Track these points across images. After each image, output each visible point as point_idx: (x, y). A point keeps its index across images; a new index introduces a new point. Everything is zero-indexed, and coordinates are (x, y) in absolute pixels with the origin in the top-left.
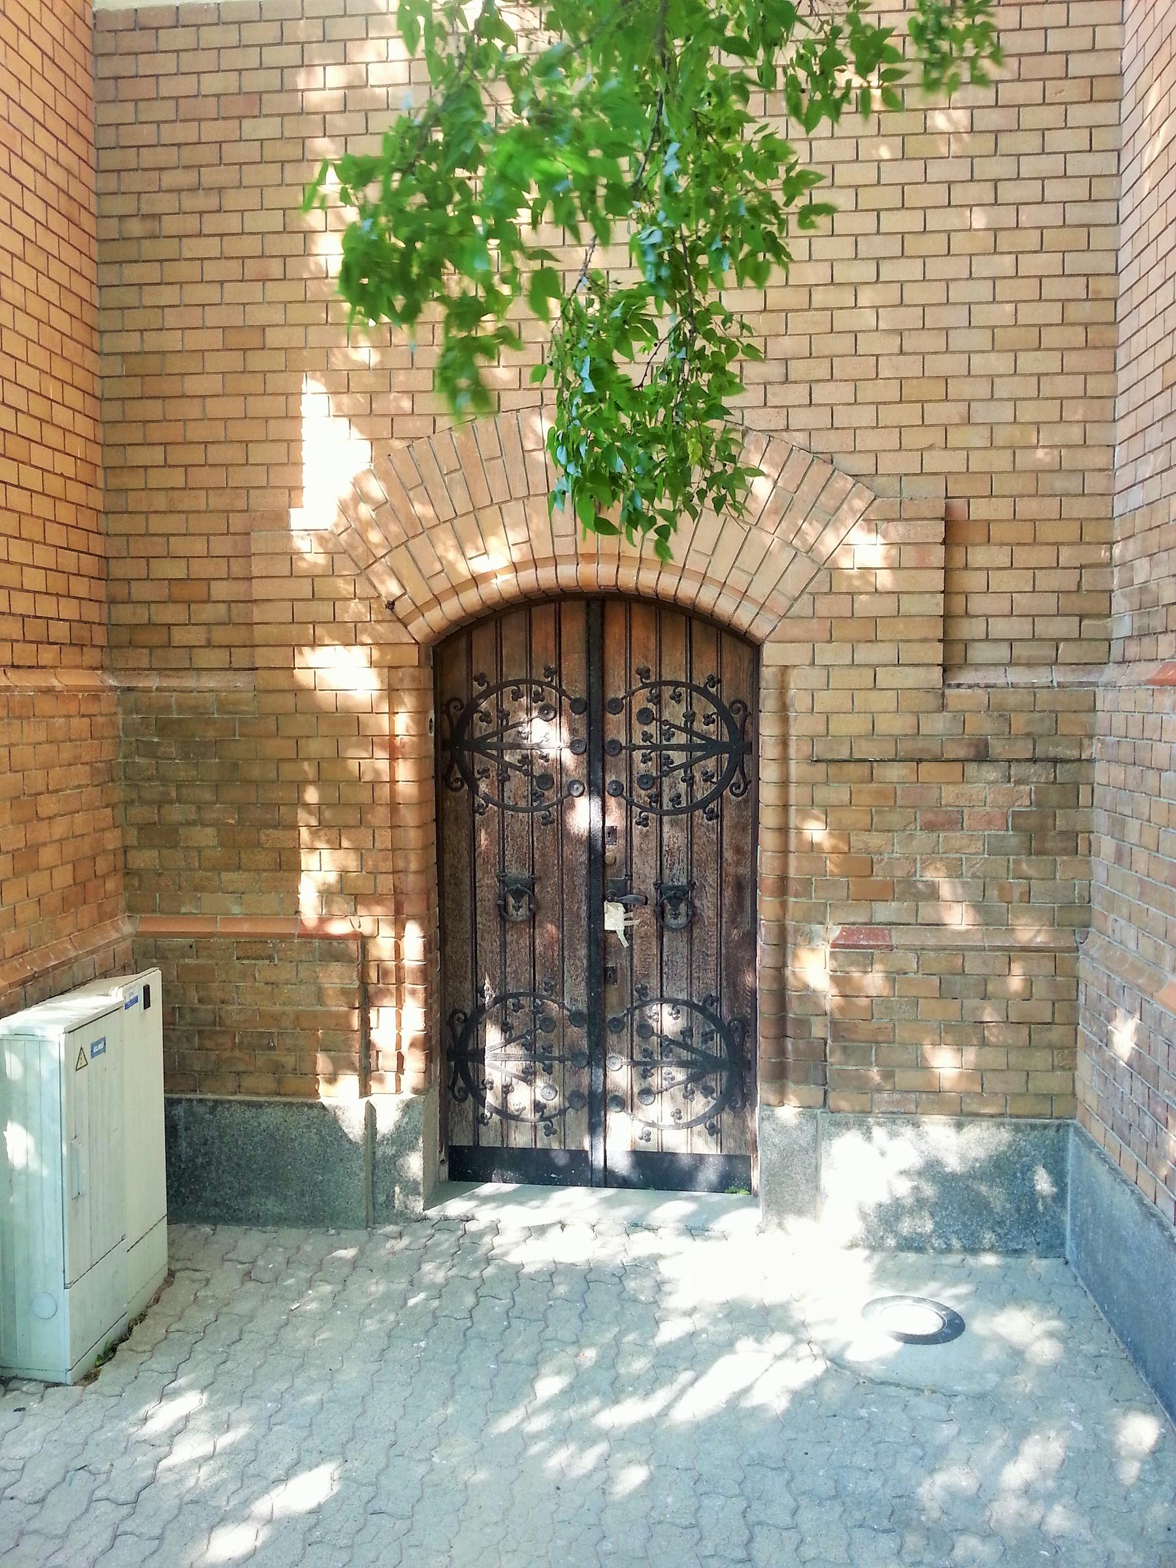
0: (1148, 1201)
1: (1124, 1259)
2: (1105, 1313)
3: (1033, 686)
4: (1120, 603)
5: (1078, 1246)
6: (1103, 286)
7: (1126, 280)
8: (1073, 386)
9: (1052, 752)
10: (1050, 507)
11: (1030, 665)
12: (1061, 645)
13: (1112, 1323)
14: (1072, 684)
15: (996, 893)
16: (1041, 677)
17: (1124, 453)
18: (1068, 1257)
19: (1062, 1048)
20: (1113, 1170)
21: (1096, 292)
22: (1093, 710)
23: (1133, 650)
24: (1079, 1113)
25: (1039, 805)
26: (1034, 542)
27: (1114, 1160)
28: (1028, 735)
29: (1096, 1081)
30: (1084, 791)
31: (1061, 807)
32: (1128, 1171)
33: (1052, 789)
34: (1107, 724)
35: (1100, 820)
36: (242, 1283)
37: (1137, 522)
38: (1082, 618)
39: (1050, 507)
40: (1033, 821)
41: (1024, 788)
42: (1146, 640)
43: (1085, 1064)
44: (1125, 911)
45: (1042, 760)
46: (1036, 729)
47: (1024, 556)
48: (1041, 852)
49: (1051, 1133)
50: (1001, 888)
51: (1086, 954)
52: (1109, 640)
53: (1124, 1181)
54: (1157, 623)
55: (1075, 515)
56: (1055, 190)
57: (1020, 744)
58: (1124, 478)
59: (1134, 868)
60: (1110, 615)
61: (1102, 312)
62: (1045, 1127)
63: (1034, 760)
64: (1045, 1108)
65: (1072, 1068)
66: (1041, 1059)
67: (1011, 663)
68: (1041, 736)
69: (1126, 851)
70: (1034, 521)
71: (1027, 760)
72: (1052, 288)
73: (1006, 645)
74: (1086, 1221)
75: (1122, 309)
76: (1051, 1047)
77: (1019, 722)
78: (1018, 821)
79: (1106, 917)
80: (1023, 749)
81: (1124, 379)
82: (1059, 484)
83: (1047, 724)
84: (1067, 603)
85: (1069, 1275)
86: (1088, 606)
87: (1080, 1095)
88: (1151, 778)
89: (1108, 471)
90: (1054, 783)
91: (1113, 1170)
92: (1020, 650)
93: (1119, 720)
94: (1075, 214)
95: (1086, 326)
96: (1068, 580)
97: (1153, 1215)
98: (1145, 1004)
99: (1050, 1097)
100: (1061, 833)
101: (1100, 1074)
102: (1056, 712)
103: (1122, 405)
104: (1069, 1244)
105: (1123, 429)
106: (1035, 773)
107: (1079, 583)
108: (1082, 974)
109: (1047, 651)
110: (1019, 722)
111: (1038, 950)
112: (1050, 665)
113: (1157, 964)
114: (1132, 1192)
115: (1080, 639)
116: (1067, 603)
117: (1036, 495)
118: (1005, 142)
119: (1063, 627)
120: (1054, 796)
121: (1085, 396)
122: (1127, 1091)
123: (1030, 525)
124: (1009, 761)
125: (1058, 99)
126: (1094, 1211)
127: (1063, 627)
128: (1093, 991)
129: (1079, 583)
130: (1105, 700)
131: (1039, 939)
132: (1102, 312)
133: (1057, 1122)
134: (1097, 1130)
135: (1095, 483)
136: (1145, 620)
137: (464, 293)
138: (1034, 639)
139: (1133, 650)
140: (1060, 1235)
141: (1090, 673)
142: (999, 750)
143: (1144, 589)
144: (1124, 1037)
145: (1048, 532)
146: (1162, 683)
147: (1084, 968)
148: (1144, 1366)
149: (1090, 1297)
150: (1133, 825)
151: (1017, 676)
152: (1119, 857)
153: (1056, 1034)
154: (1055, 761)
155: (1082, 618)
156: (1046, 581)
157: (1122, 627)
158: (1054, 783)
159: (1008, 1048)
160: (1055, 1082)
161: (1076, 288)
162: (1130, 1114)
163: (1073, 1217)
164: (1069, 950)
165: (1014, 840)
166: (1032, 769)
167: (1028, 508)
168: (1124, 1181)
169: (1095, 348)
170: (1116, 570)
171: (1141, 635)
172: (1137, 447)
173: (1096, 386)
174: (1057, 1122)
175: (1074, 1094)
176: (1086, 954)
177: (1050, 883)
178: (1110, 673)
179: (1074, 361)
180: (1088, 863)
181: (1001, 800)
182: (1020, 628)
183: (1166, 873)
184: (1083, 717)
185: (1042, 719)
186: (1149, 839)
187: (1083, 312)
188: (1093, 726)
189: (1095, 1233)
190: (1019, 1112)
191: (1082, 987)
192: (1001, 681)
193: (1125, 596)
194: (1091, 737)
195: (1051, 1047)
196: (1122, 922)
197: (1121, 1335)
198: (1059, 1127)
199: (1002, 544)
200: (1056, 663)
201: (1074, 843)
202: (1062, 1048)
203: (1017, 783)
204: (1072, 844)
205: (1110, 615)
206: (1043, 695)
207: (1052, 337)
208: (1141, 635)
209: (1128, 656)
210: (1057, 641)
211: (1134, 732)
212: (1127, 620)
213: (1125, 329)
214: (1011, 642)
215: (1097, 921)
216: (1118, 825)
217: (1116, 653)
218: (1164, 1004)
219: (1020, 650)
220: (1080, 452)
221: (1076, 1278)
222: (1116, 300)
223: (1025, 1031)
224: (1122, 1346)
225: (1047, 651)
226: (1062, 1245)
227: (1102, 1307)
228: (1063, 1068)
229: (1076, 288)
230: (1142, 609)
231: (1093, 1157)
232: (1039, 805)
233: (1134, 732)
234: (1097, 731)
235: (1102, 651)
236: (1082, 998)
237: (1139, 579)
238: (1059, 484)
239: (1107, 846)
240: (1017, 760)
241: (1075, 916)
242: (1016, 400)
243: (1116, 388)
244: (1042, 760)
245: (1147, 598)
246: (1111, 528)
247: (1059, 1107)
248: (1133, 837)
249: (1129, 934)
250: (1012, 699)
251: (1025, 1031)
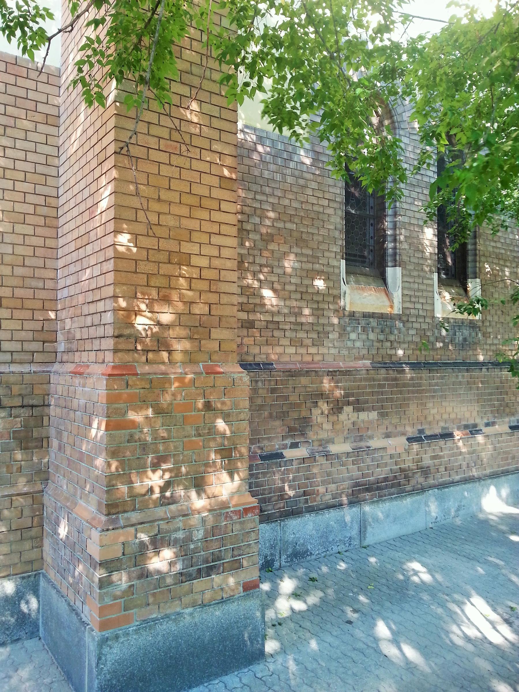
0: (72, 603)
1: (63, 632)
2: (56, 659)
3: (22, 373)
4: (60, 337)
5: (44, 629)
6: (52, 202)
7: (62, 201)
8: (40, 242)
9: (31, 402)
10: (29, 293)
11: (21, 363)
12: (35, 354)
13: (58, 663)
14: (40, 372)
15: (5, 469)
16: (26, 368)
17: (61, 273)
18: (41, 636)
19: (36, 538)
20: (58, 591)
21: (49, 203)
22: (49, 383)
23: (65, 358)
24: (45, 567)
25: (25, 427)
26: (22, 308)
27: (59, 587)
28: (20, 395)
29: (51, 552)
30: (46, 419)
31: (35, 427)
32: (64, 591)
33: (31, 419)
34: (54, 389)
35: (52, 432)
36: (103, 374)
37: (67, 303)
38: (44, 342)
39: (29, 293)
40: (22, 434)
41: (18, 419)
42: (70, 353)
43: (47, 543)
44: (62, 472)
45: (26, 406)
46: (23, 392)
47: (17, 314)
48: (26, 449)
49: (32, 579)
50: (8, 467)
51: (46, 493)
52: (56, 352)
53: (62, 596)
54: (74, 347)
55: (41, 297)
56: (31, 157)
57: (16, 399)
58: (61, 283)
59: (66, 453)
60: (56, 342)
61: (52, 212)
62: (29, 576)
63: (23, 407)
64: (29, 568)
65: (41, 546)
66: (27, 545)
67: (12, 362)
68: (26, 395)
69: (63, 446)
70: (22, 298)
71: (20, 406)
72: (30, 198)
73: (9, 354)
74: (47, 618)
75: (60, 213)
76: (32, 538)
77: (16, 389)
78: (16, 435)
79: (55, 475)
80: (18, 402)
81: (61, 242)
82: (34, 283)
83: (29, 390)
84: (37, 335)
85: (41, 645)
86: (47, 336)
87: (45, 559)
88: (72, 413)
89: (55, 279)
90: (32, 416)
91: (58, 591)
92: (16, 356)
93: (60, 388)
94: (40, 169)
95: (45, 217)
96: (38, 326)
97: (74, 610)
98: (70, 515)
99: (31, 562)
100: (36, 439)
101: (52, 548)
102: (33, 384)
103: (60, 253)
104: (41, 629)
105: (61, 263)
106: (23, 412)
107: (43, 327)
108: (45, 503)
109: (29, 357)
110: (16, 389)
111: (26, 494)
112: (30, 363)
113: (75, 495)
114: (66, 600)
115: (43, 352)
116: (37, 335)
117: (23, 287)
118: (9, 131)
119: (36, 346)
120: (32, 422)
121: (44, 247)
122: (63, 554)
123: (20, 300)
124: (11, 407)
125: (32, 119)
126: (51, 612)
127: (36, 346)
128: (50, 510)
129: (43, 327)
130: (53, 379)
131: (25, 489)
132: (52, 212)
133: (34, 573)
134: (52, 574)
135: (49, 284)
136: (70, 345)
137: (448, 215)
138: (22, 351)
139: (65, 358)
140: (37, 626)
141: (48, 367)
142: (5, 403)
143: (69, 332)
144: (63, 531)
145: (28, 304)
146: (75, 373)
147: (46, 499)
148: (71, 681)
149: (50, 653)
150: (65, 434)
151: (15, 368)
152: (60, 449)
153: (34, 532)
154: (32, 406)
155: (44, 342)
156: (28, 325)
157: (61, 347)
158: (32, 416)
159: (11, 543)
160: (33, 555)
161: (40, 200)
162: (64, 565)
163: (43, 616)
164: (39, 492)
165: (13, 443)
166: (22, 410)
167: (19, 293)
168: (62, 596)
169: (49, 227)
170: (59, 322)
171: (68, 351)
172: (66, 271)
173: (50, 243)
174: (34, 573)
175: (42, 558)
176: (46, 493)
177: (30, 462)
178: (56, 367)
179: (39, 231)
180: (48, 451)
181: (7, 426)
182: (17, 346)
183: (77, 456)
184: (45, 386)
185: (26, 388)
186: (71, 441)
187: (44, 211)
188: (49, 390)
189: (51, 622)
190: (17, 572)
191: (45, 508)
192: (7, 370)
193: (62, 334)
194: (48, 395)
195: (32, 538)
196: (61, 477)
197: (62, 668)
198: (35, 575)
199: (7, 308)
200: (32, 362)
201: (42, 443)
202: (36, 538)
203: (15, 417)
204: (39, 444)
205: (56, 342)
206: (26, 377)
207: (29, 219)
208: (68, 351)
209: (64, 360)
210: (33, 352)
211: (65, 394)
212: (63, 344)
213: (62, 221)
214: (12, 352)
215: (52, 477)
216: (59, 433)
217: (59, 358)
218: (77, 514)
219: (16, 356)
220: (42, 271)
221: (44, 645)
222: (57, 208)
223: (19, 533)
224: (62, 674)
225: (29, 357)
226: (38, 630)
227: (55, 657)
228: (37, 547)
229: (40, 200)
230: (69, 340)
231: (50, 587)
232: (25, 427)
233: (65, 394)
234: (51, 392)
235: (53, 357)
236: (45, 513)
237: (67, 327)
238: (34, 283)
239: (55, 443)
240: (15, 407)
241: (43, 475)
242: (13, 244)
243: (58, 245)
244: (26, 406)
245: (71, 336)
246: (57, 304)
247: (35, 566)
248: (65, 440)
249: (64, 482)
250: (12, 379)
251: (19, 533)
